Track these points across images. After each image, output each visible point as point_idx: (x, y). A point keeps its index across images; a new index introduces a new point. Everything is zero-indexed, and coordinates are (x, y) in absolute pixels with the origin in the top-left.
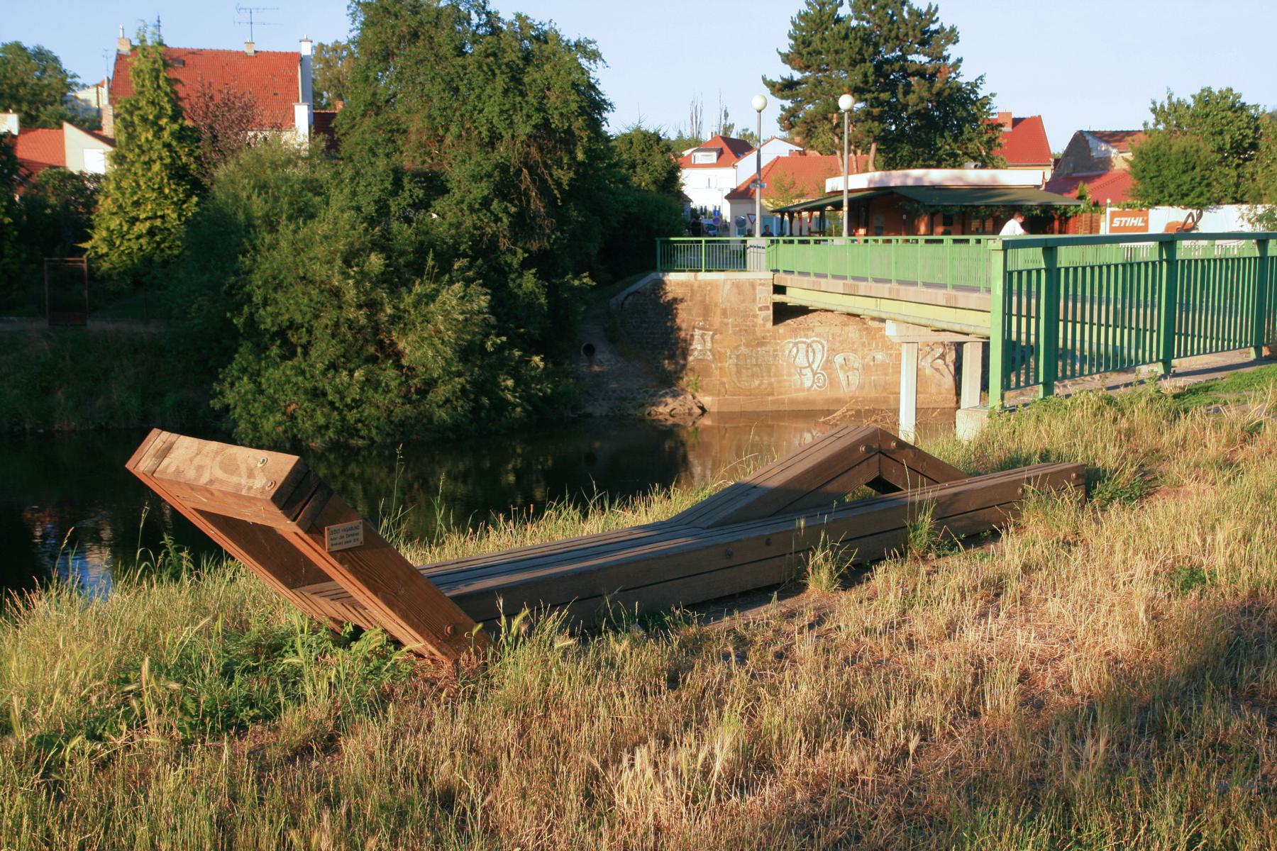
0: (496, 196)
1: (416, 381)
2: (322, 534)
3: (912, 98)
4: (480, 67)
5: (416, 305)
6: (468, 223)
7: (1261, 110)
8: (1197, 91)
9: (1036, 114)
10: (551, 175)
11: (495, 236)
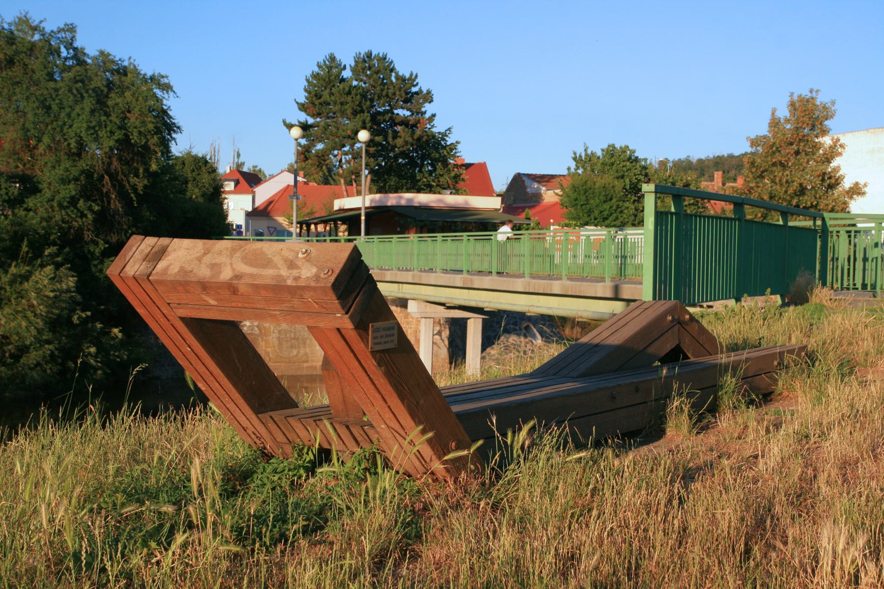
0: (81, 196)
1: (10, 347)
2: (367, 330)
3: (399, 142)
4: (70, 91)
5: (12, 283)
6: (58, 217)
7: (648, 162)
8: (605, 146)
9: (481, 161)
10: (129, 183)
11: (80, 229)
